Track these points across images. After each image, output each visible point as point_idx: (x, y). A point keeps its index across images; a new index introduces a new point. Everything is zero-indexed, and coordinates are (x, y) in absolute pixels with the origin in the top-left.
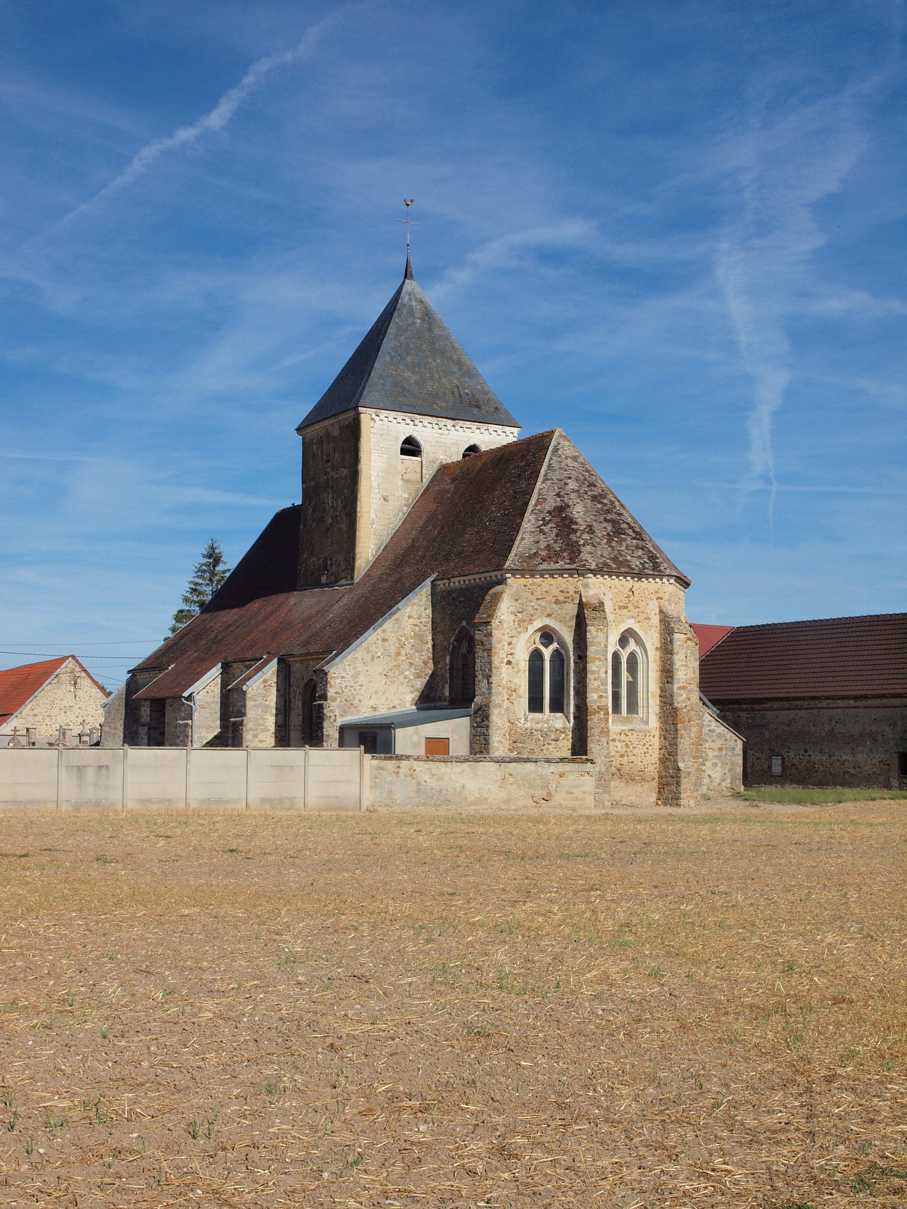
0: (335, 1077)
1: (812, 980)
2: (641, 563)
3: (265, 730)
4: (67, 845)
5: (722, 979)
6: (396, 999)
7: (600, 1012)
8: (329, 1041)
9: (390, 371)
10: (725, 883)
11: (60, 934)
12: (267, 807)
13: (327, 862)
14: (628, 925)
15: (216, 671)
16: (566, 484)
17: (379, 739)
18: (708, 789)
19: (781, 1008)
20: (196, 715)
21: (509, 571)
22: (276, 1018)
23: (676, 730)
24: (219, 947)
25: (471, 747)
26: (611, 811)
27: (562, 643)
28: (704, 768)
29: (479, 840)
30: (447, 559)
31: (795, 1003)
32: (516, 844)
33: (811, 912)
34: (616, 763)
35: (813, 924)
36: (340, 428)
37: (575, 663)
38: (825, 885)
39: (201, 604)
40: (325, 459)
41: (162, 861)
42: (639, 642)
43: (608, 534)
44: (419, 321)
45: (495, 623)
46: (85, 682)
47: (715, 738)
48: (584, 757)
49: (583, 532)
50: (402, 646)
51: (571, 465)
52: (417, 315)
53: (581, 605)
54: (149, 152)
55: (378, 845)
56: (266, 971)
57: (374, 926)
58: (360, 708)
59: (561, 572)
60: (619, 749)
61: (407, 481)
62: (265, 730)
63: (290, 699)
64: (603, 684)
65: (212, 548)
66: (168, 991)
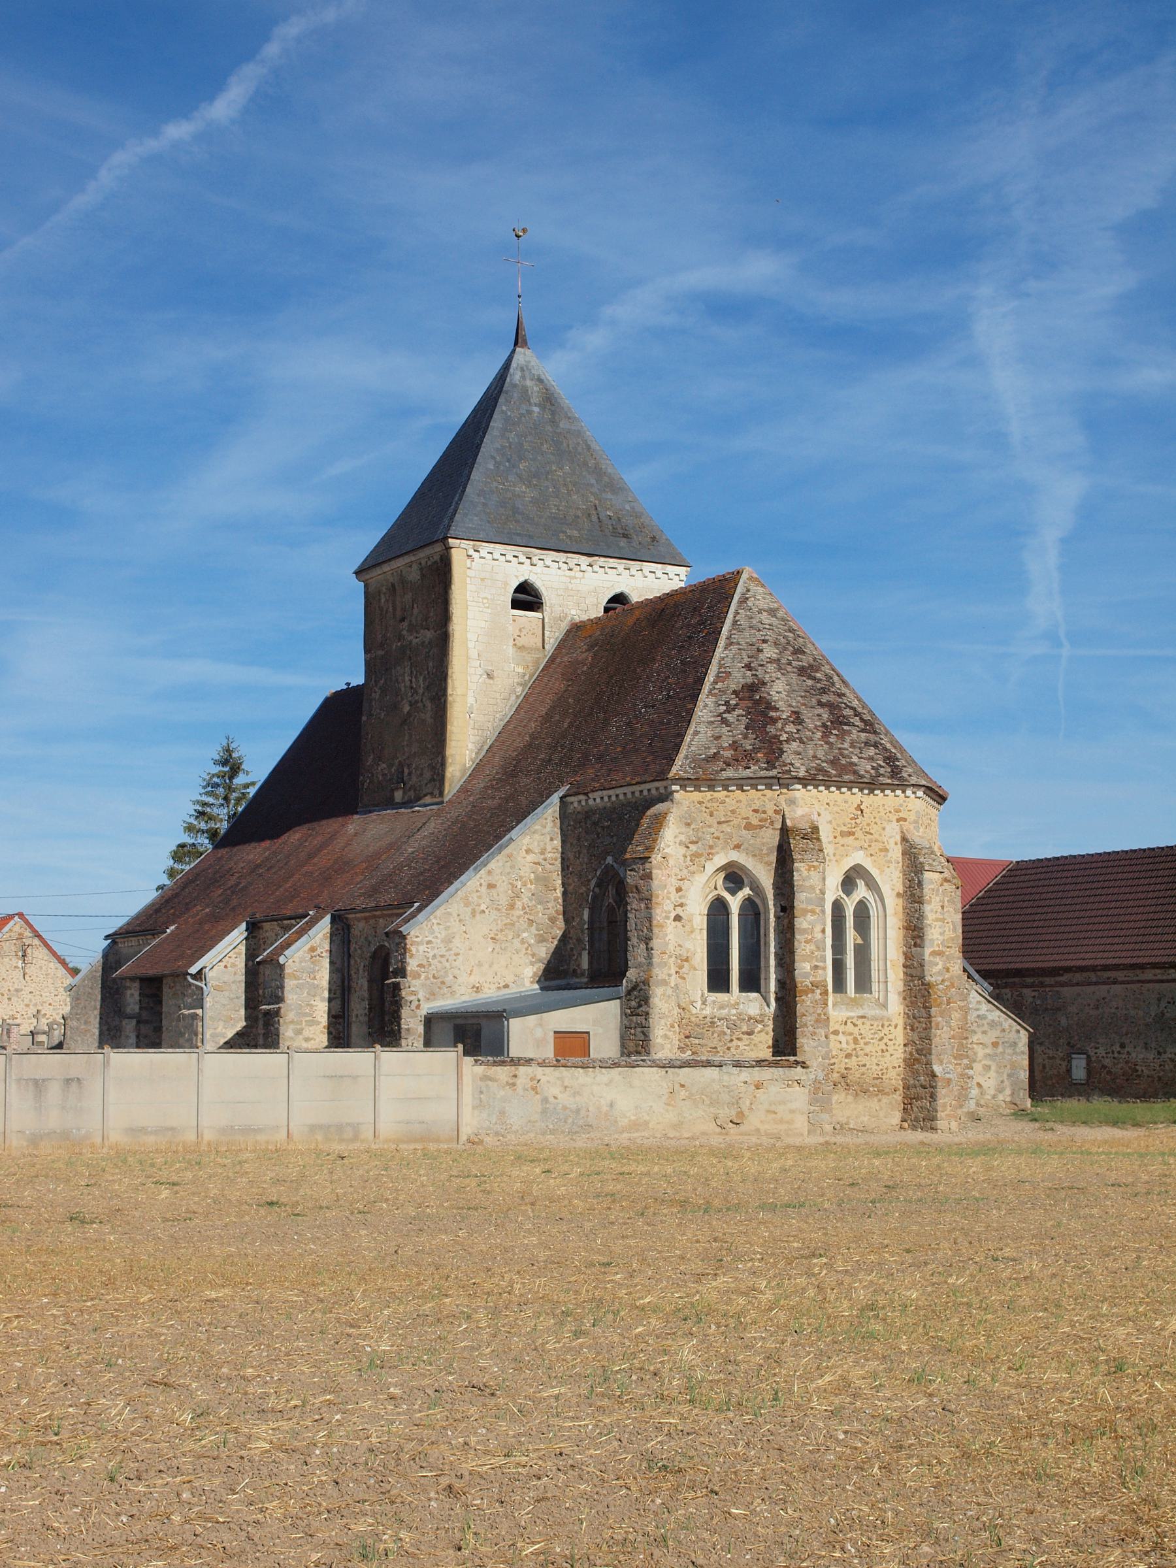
0: (458, 1535)
1: (1152, 1386)
2: (873, 768)
3: (313, 1022)
4: (22, 1198)
5: (1019, 1385)
6: (537, 1420)
7: (841, 1436)
8: (444, 1481)
9: (495, 484)
10: (1012, 1245)
11: (28, 1330)
12: (319, 1138)
13: (414, 1218)
14: (872, 1307)
15: (238, 934)
16: (760, 651)
17: (485, 1033)
18: (978, 1105)
19: (1107, 1427)
20: (208, 1002)
22: (363, 1449)
24: (268, 1345)
25: (623, 1046)
26: (833, 1140)
28: (971, 1072)
29: (639, 1184)
30: (583, 764)
31: (1128, 1419)
32: (695, 1189)
33: (1143, 1285)
34: (840, 1067)
35: (1148, 1304)
36: (421, 569)
37: (777, 918)
38: (1161, 1246)
39: (212, 835)
40: (399, 614)
41: (168, 1220)
42: (872, 885)
44: (536, 409)
45: (656, 859)
46: (39, 954)
47: (986, 1028)
48: (792, 1058)
51: (767, 622)
52: (535, 400)
53: (785, 831)
54: (123, 159)
55: (489, 1193)
56: (341, 1380)
57: (495, 1313)
58: (455, 988)
59: (754, 782)
60: (844, 1045)
61: (522, 648)
62: (313, 1022)
63: (349, 975)
65: (228, 751)
66: (199, 1412)
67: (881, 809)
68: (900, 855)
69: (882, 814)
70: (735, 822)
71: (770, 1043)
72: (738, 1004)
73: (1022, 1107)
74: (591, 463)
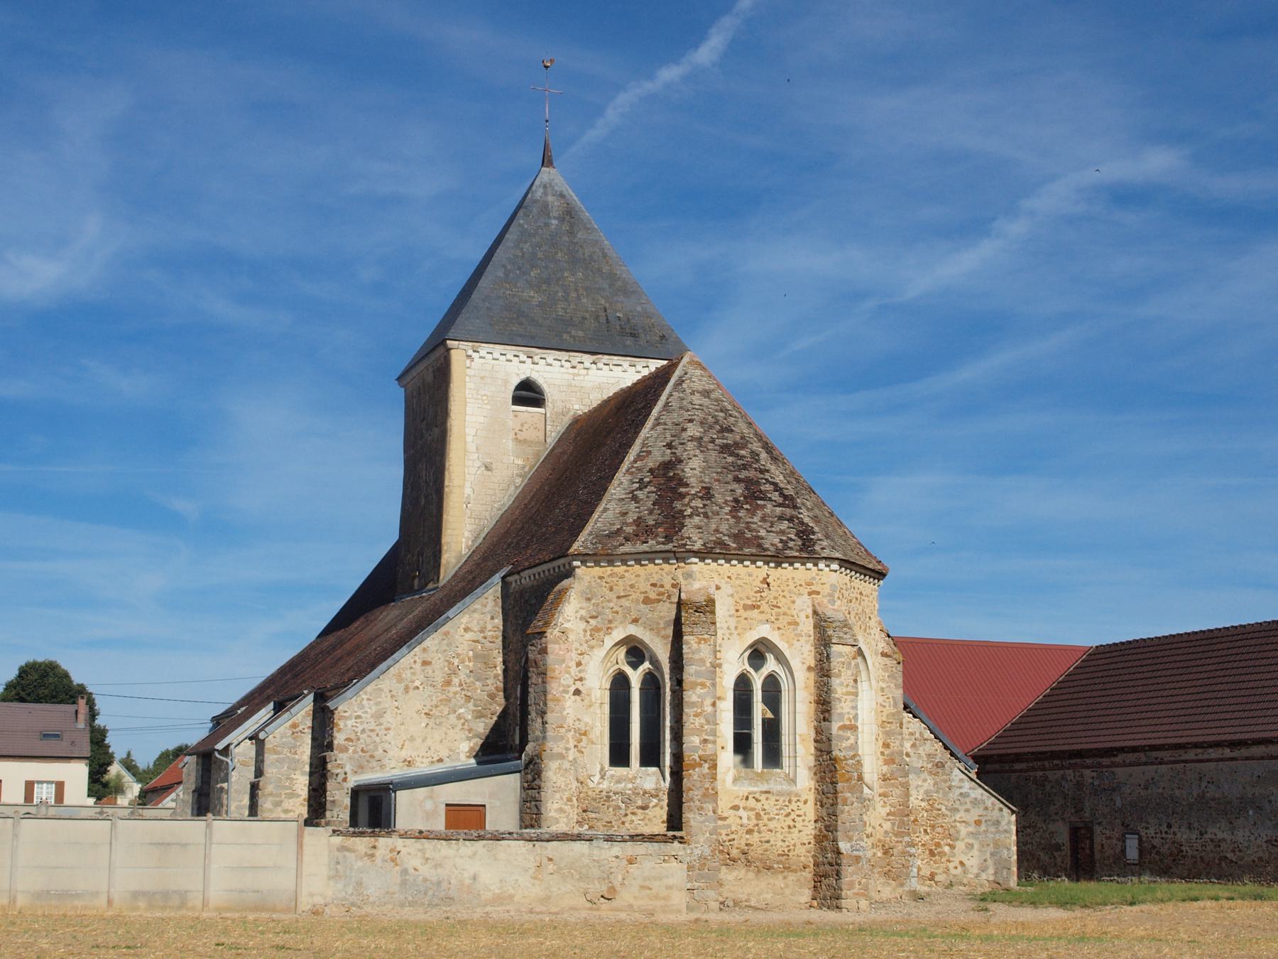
2: (781, 541)
3: (293, 795)
16: (684, 430)
21: (577, 556)
23: (836, 792)
25: (522, 819)
27: (655, 662)
42: (781, 659)
43: (736, 500)
44: (554, 222)
45: (552, 633)
47: (969, 806)
49: (695, 496)
50: (455, 672)
52: (554, 213)
53: (680, 604)
54: (625, 100)
58: (386, 761)
59: (651, 556)
60: (745, 821)
62: (293, 795)
64: (708, 722)
67: (791, 583)
69: (792, 587)
70: (634, 596)
71: (665, 818)
72: (635, 778)
74: (606, 269)
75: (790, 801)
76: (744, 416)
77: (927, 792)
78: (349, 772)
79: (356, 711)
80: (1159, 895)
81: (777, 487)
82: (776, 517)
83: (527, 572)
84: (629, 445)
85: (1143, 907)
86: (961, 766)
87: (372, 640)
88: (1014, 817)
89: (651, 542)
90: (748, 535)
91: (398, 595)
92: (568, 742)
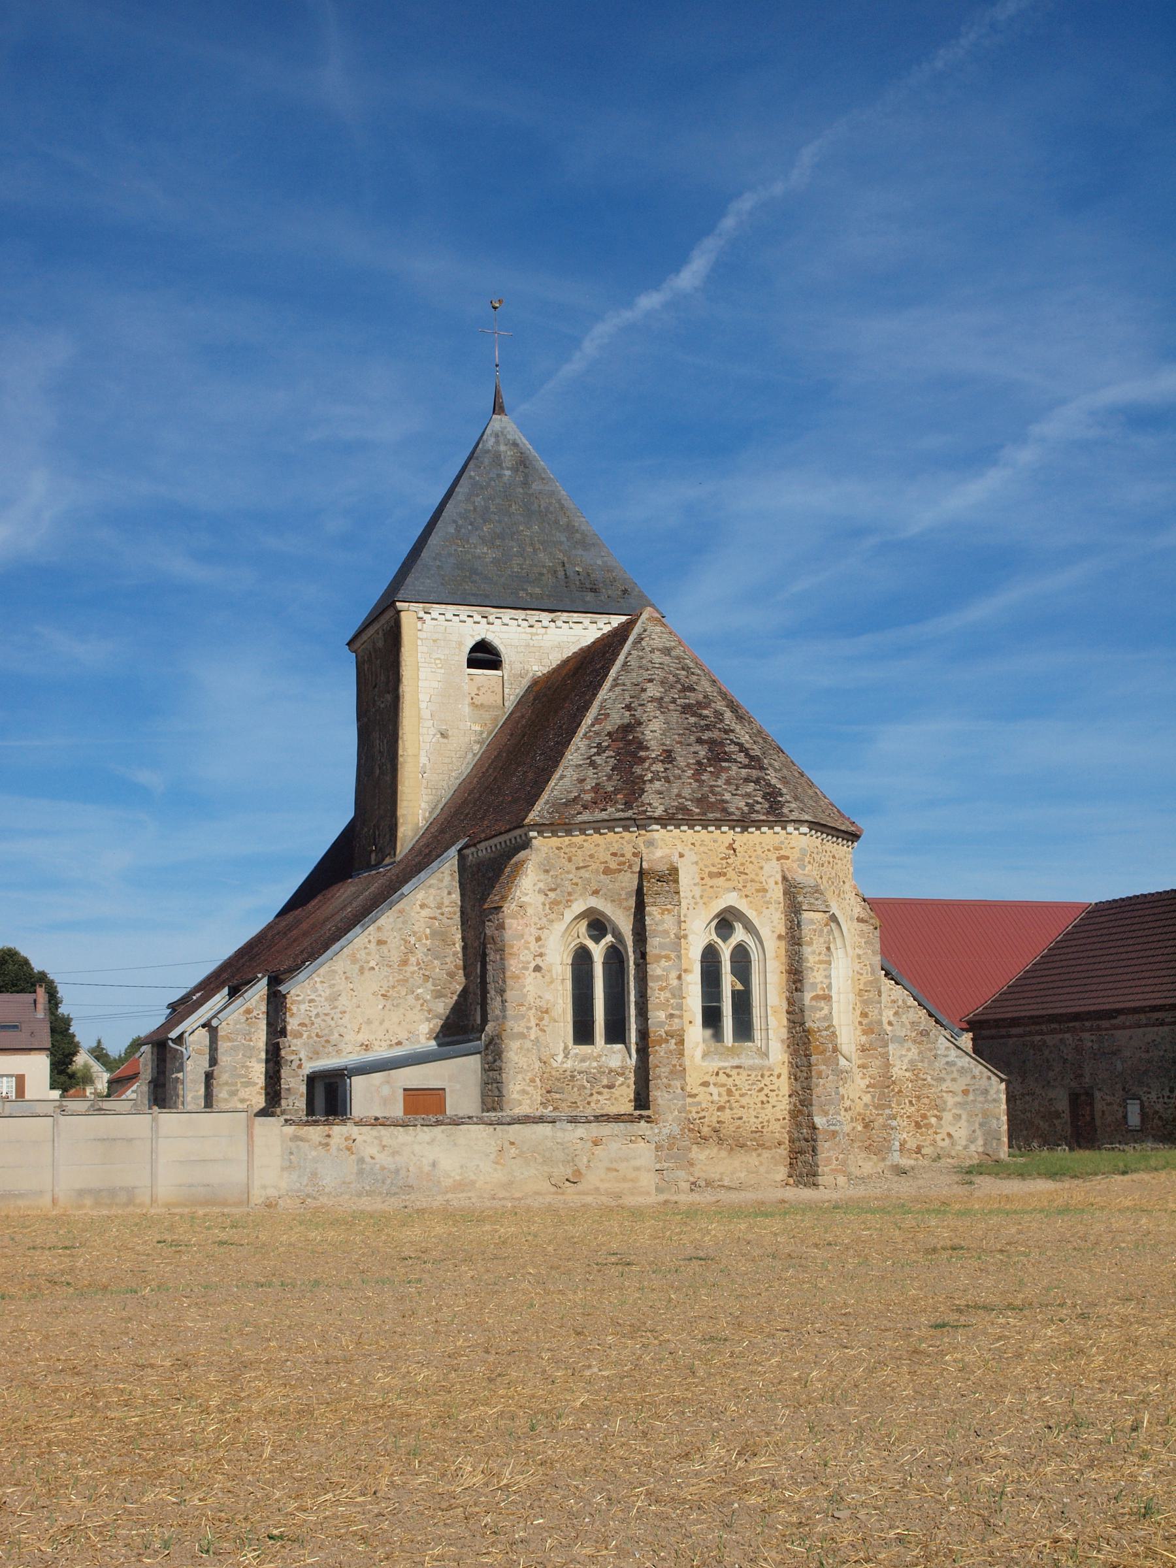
3: (249, 1083)
9: (454, 547)
16: (644, 690)
23: (810, 1065)
25: (483, 1103)
27: (618, 935)
42: (750, 927)
43: (699, 763)
44: (508, 473)
45: (509, 908)
47: (955, 1075)
50: (411, 951)
52: (508, 463)
53: (642, 873)
54: (600, 334)
58: (342, 1046)
59: (610, 824)
60: (716, 1098)
62: (249, 1083)
64: (674, 996)
67: (758, 848)
68: (781, 895)
69: (759, 852)
71: (632, 1096)
72: (600, 1056)
73: (995, 1158)
75: (762, 1076)
76: (707, 674)
77: (911, 1062)
78: (305, 1059)
79: (308, 993)
80: (1153, 1163)
81: (742, 749)
82: (739, 777)
83: (483, 844)
84: (586, 707)
85: (1135, 1176)
86: (947, 1033)
87: (327, 919)
88: (1003, 1086)
89: (610, 810)
90: (712, 799)
91: (355, 867)
92: (529, 1020)
